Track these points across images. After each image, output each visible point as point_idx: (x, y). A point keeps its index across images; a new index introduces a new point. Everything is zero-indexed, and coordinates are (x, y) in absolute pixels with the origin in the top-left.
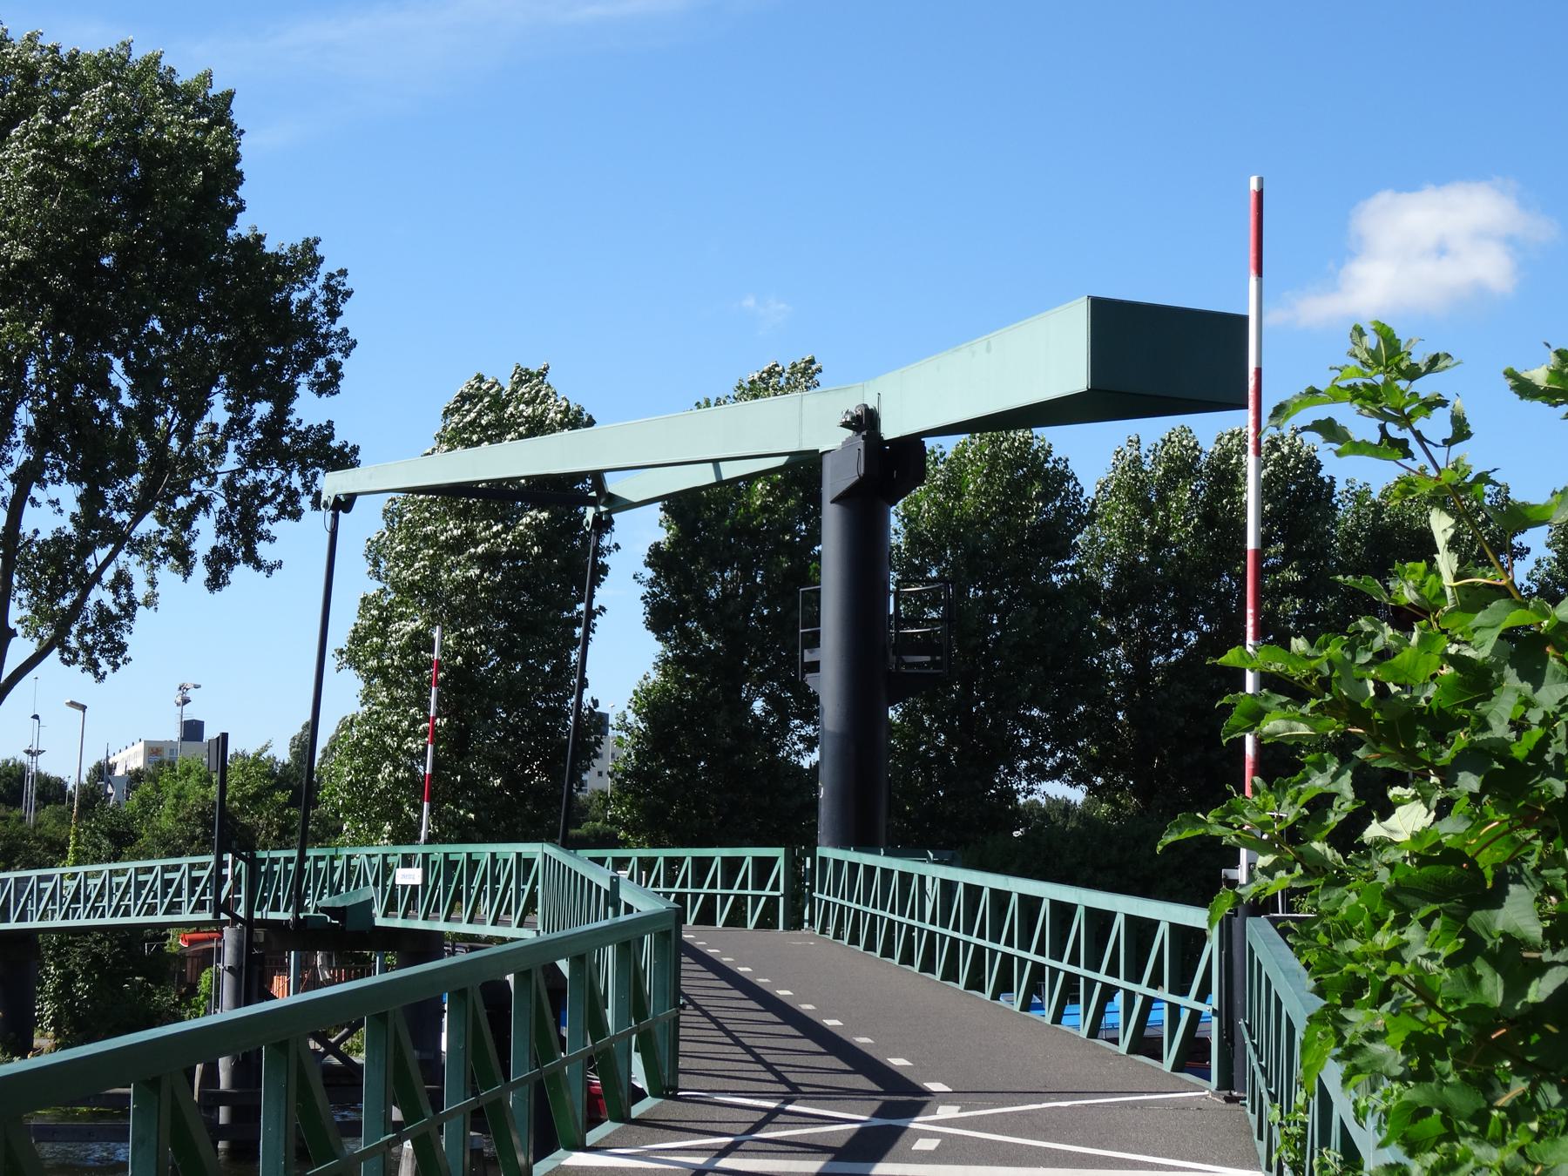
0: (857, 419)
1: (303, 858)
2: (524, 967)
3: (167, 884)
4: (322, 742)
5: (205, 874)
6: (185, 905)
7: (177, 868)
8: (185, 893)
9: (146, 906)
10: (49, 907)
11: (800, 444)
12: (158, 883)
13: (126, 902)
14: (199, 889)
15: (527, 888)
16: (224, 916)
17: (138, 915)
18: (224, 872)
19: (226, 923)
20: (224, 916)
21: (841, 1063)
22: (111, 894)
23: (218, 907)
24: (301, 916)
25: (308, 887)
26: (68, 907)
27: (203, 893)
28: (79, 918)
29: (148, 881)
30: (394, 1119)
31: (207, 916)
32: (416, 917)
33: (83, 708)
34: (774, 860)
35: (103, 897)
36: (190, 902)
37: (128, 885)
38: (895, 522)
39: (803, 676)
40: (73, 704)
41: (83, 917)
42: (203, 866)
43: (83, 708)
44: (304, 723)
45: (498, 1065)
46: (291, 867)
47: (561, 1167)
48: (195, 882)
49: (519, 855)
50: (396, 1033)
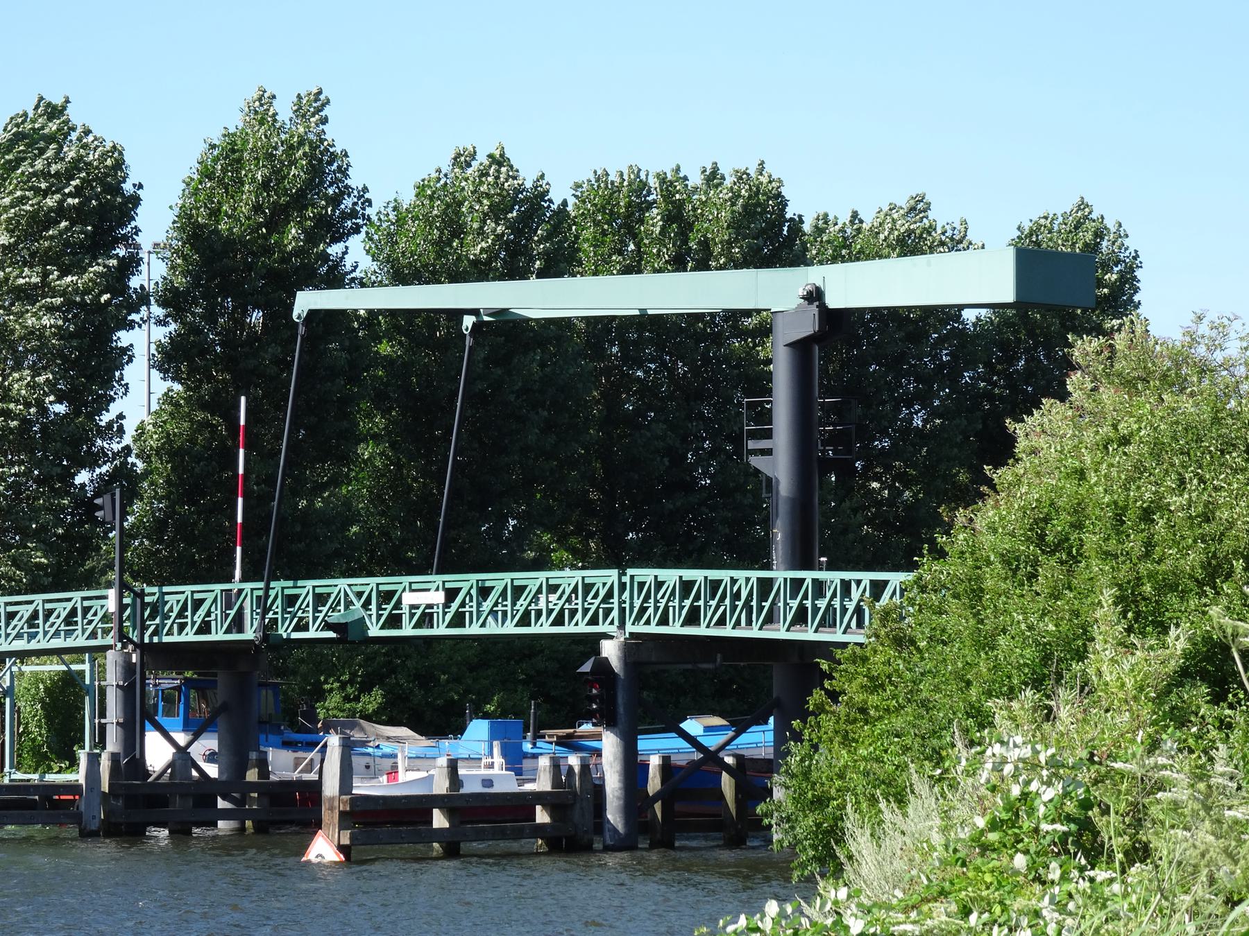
0: (810, 293)
1: (267, 588)
6: (405, 618)
8: (373, 606)
9: (296, 619)
11: (929, 264)
12: (310, 597)
15: (767, 605)
17: (708, 626)
26: (174, 622)
28: (577, 624)
29: (396, 591)
30: (462, 845)
32: (807, 631)
35: (675, 598)
36: (379, 617)
39: (747, 458)
41: (654, 623)
45: (619, 793)
47: (318, 825)
49: (706, 578)
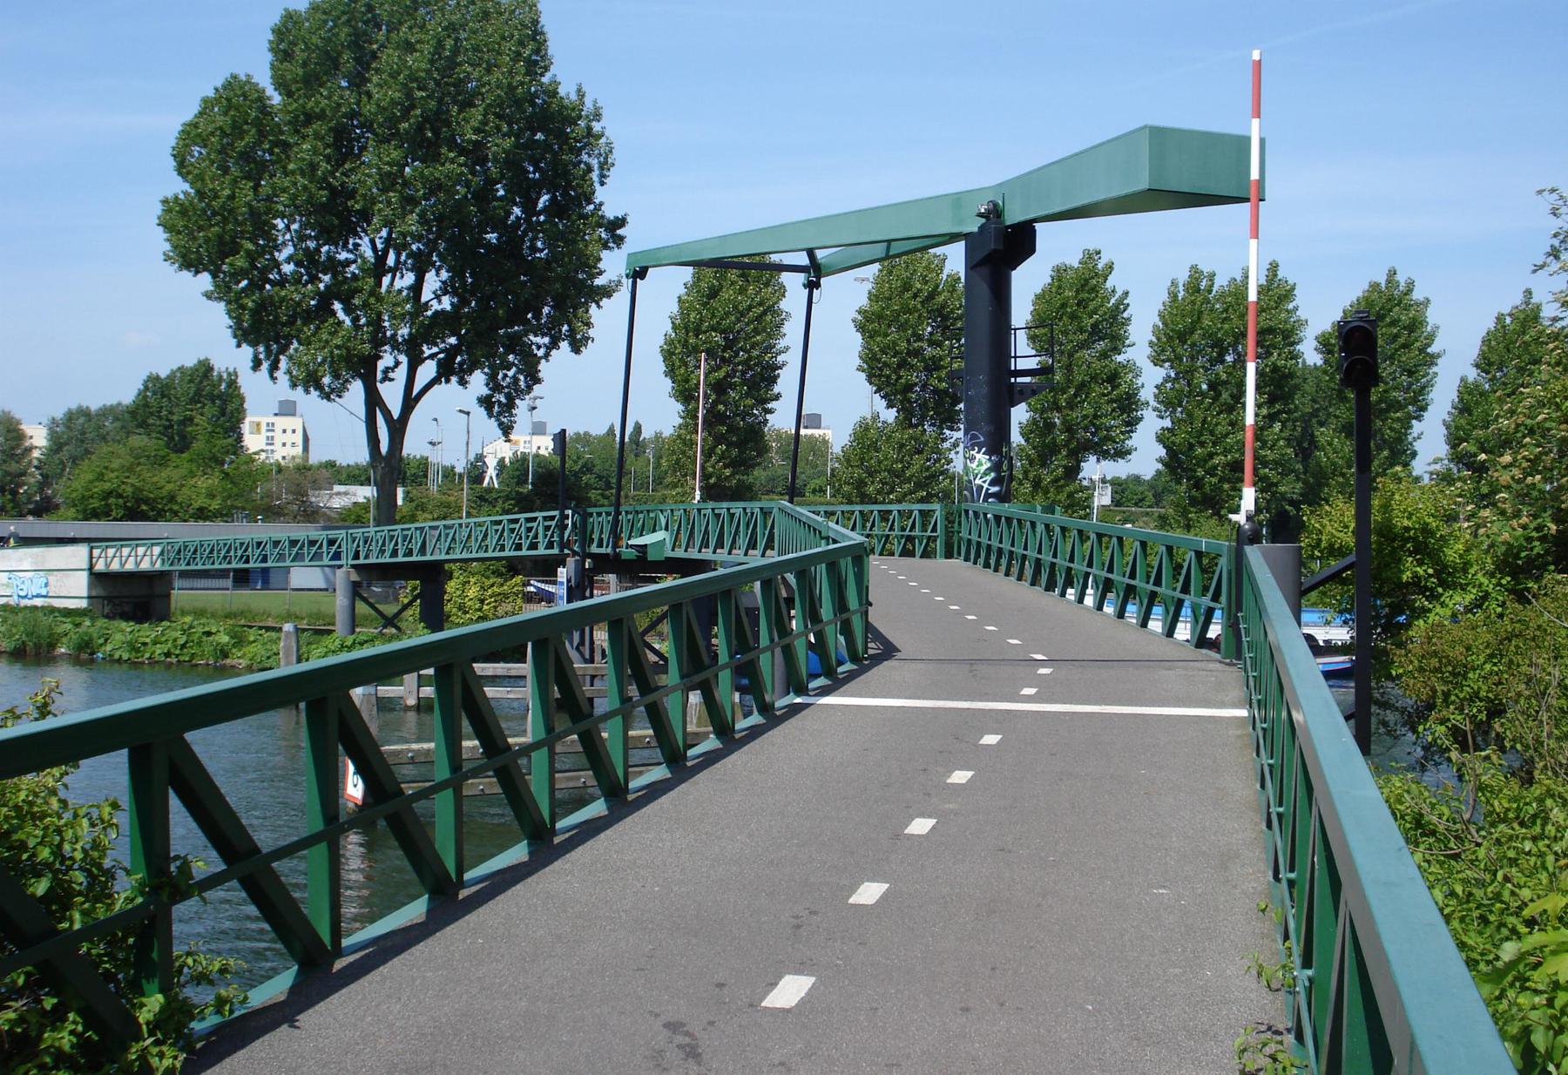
2: (766, 575)
3: (530, 530)
4: (627, 440)
5: (553, 523)
6: (325, 555)
7: (516, 521)
10: (438, 546)
13: (501, 542)
14: (550, 533)
16: (566, 551)
18: (566, 522)
19: (568, 555)
20: (566, 551)
21: (171, 802)
22: (236, 549)
23: (562, 546)
24: (618, 550)
25: (621, 532)
27: (552, 536)
31: (556, 551)
33: (468, 413)
34: (934, 511)
37: (503, 530)
38: (1372, 445)
40: (461, 411)
41: (474, 551)
42: (552, 518)
43: (468, 413)
44: (246, 400)
46: (610, 518)
48: (547, 528)
50: (688, 618)
